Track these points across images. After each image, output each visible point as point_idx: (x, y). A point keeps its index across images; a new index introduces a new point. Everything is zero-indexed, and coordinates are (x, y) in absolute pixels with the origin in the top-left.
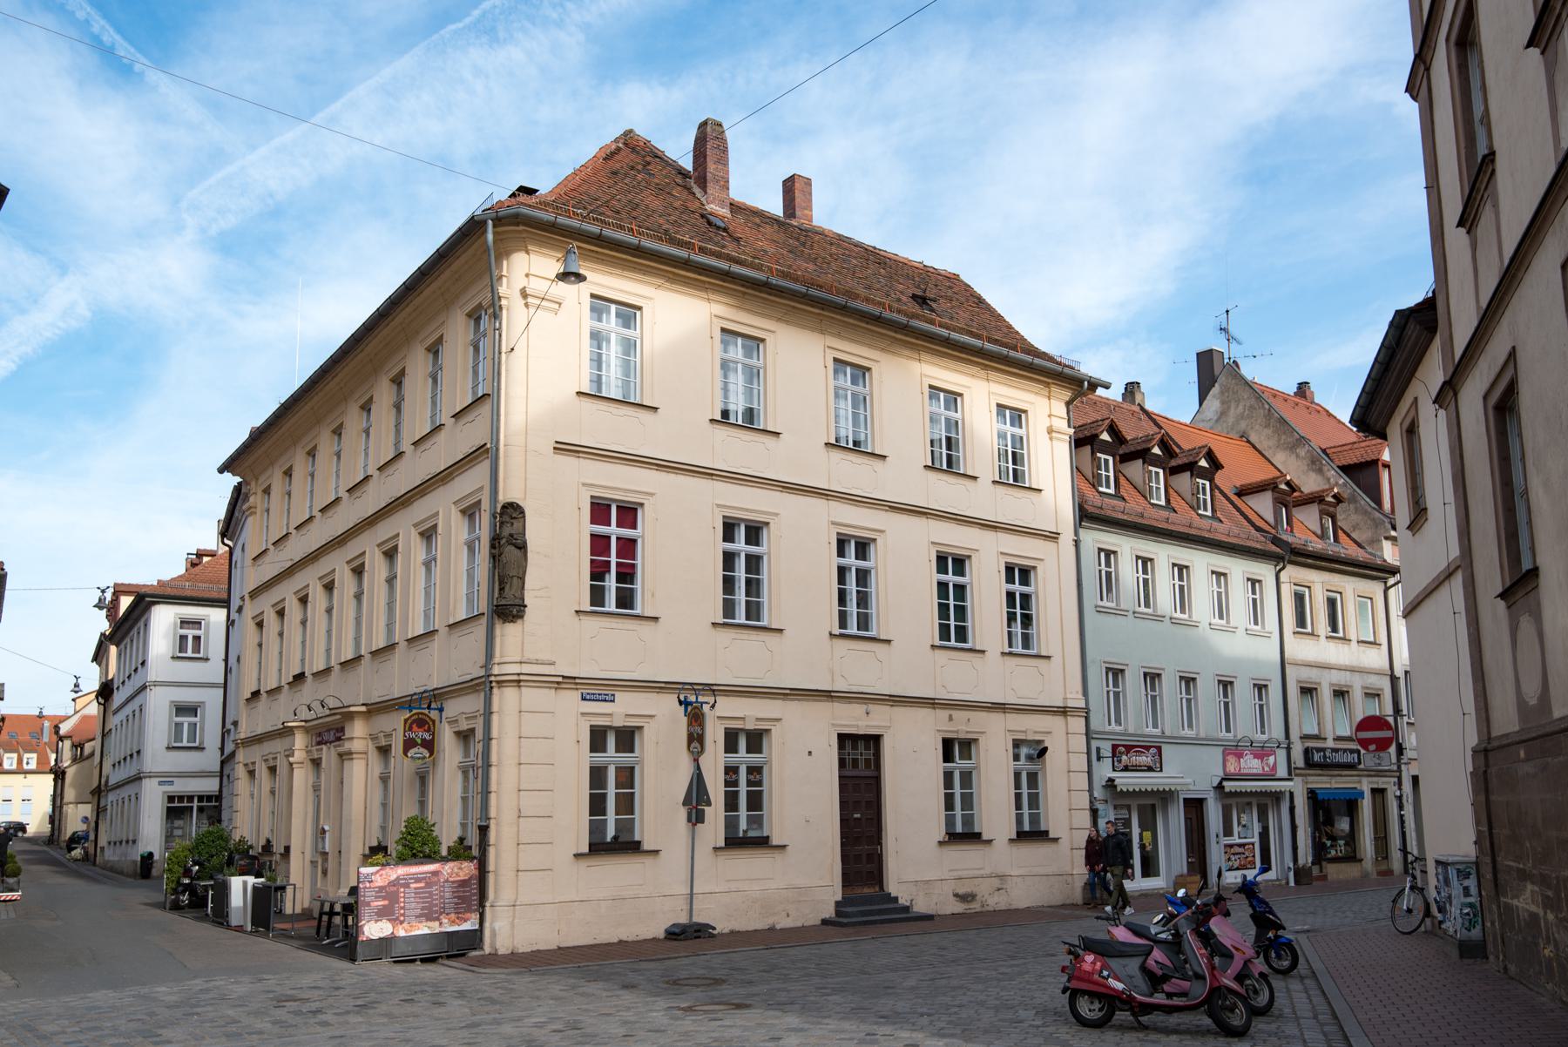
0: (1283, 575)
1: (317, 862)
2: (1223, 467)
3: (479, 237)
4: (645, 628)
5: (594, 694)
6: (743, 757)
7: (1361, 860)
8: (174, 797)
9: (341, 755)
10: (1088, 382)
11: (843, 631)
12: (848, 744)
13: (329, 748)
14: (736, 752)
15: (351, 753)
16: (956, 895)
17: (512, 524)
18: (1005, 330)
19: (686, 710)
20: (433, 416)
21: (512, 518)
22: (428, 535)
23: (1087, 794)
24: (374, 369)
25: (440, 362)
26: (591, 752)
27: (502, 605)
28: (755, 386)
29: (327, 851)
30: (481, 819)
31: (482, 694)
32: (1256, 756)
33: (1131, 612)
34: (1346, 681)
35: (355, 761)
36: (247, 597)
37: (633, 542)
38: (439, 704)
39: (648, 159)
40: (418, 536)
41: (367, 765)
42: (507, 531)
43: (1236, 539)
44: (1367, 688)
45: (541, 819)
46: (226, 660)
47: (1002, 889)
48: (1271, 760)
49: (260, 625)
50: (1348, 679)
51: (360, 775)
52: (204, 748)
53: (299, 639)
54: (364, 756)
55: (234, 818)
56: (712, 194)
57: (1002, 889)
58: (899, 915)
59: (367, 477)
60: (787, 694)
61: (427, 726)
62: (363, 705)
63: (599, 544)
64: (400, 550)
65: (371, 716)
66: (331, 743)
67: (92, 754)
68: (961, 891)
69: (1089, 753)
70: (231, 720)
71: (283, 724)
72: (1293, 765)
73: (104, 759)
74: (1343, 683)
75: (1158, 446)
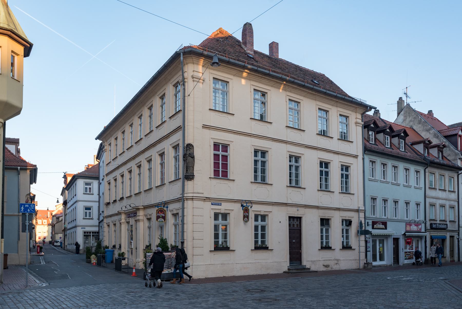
0: (427, 170)
1: (129, 251)
2: (409, 136)
3: (178, 59)
4: (230, 183)
5: (215, 203)
6: (260, 223)
7: (445, 257)
8: (85, 232)
9: (136, 221)
10: (370, 107)
12: (292, 219)
13: (132, 219)
14: (258, 221)
15: (139, 220)
16: (323, 265)
17: (190, 150)
18: (341, 91)
19: (243, 209)
20: (150, 128)
22: (149, 161)
24: (143, 104)
25: (152, 112)
26: (214, 220)
27: (187, 175)
29: (132, 247)
30: (181, 240)
31: (181, 203)
32: (416, 225)
34: (444, 203)
35: (140, 222)
36: (105, 176)
37: (227, 156)
38: (167, 206)
40: (147, 162)
41: (144, 223)
42: (188, 152)
43: (412, 158)
44: (450, 205)
45: (200, 240)
46: (99, 195)
47: (338, 264)
48: (420, 227)
49: (109, 183)
50: (445, 202)
52: (93, 219)
53: (114, 190)
54: (143, 221)
55: (104, 238)
56: (248, 47)
57: (338, 264)
59: (124, 152)
61: (163, 212)
62: (142, 206)
63: (216, 157)
64: (152, 160)
65: (145, 209)
66: (132, 217)
67: (62, 220)
68: (325, 264)
70: (102, 211)
71: (118, 211)
72: (427, 228)
73: (66, 222)
75: (389, 129)
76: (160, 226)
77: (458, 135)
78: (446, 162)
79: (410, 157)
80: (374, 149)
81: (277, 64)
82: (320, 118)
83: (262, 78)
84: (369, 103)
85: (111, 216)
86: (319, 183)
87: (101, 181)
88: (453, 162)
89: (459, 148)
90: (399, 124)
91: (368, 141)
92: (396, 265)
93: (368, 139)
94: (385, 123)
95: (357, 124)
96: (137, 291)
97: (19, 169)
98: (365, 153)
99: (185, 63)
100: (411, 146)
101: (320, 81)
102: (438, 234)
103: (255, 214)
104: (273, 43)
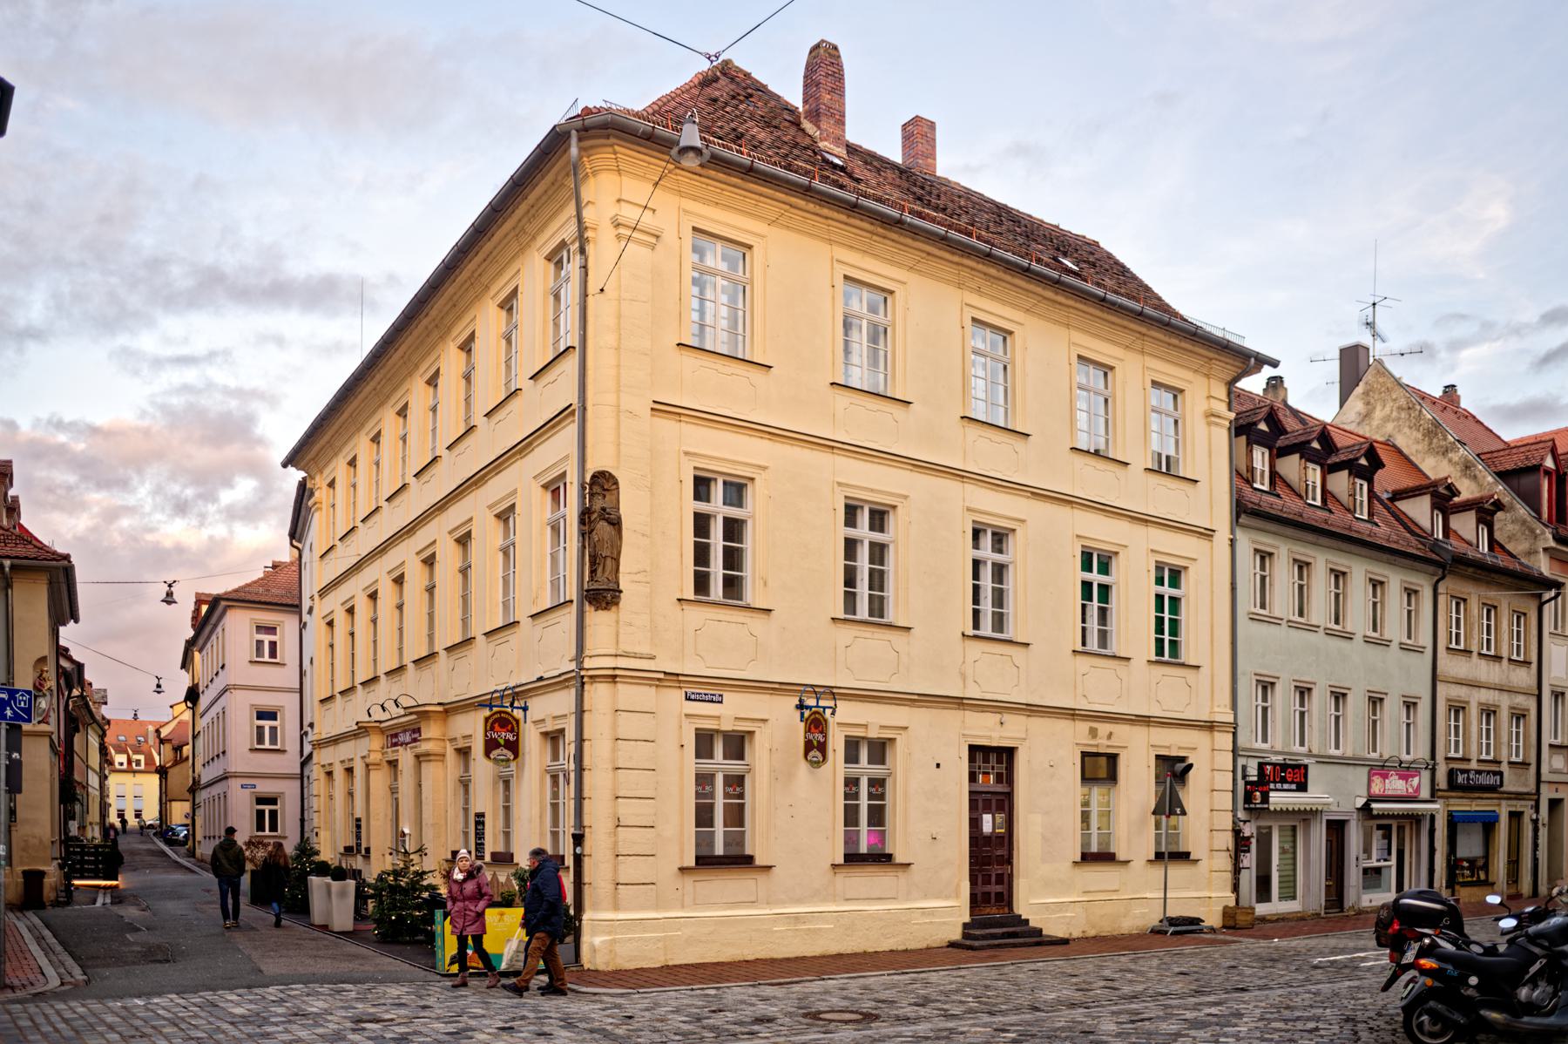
0: (1441, 589)
4: (756, 623)
6: (865, 768)
7: (1493, 884)
10: (1256, 359)
11: (977, 632)
12: (979, 756)
17: (604, 496)
19: (802, 715)
21: (605, 490)
23: (1230, 814)
28: (881, 346)
31: (573, 691)
32: (1402, 777)
33: (1285, 621)
36: (316, 597)
39: (749, 91)
44: (1514, 708)
48: (1416, 781)
49: (330, 624)
51: (440, 778)
56: (826, 130)
58: (1027, 938)
59: (436, 458)
60: (915, 700)
69: (1234, 771)
71: (357, 723)
74: (1491, 702)
76: (500, 777)
77: (1542, 469)
78: (1501, 561)
79: (1388, 540)
80: (1268, 510)
81: (930, 193)
82: (1085, 393)
83: (875, 238)
84: (1253, 343)
85: (335, 740)
86: (1080, 625)
87: (306, 617)
88: (1523, 560)
89: (1545, 515)
90: (1347, 427)
91: (1249, 482)
92: (1335, 913)
93: (1249, 475)
94: (1303, 422)
95: (1213, 419)
96: (394, 1016)
97: (7, 569)
98: (1240, 520)
99: (588, 170)
100: (1390, 505)
101: (1084, 261)
102: (1516, 806)
103: (846, 736)
104: (917, 120)
